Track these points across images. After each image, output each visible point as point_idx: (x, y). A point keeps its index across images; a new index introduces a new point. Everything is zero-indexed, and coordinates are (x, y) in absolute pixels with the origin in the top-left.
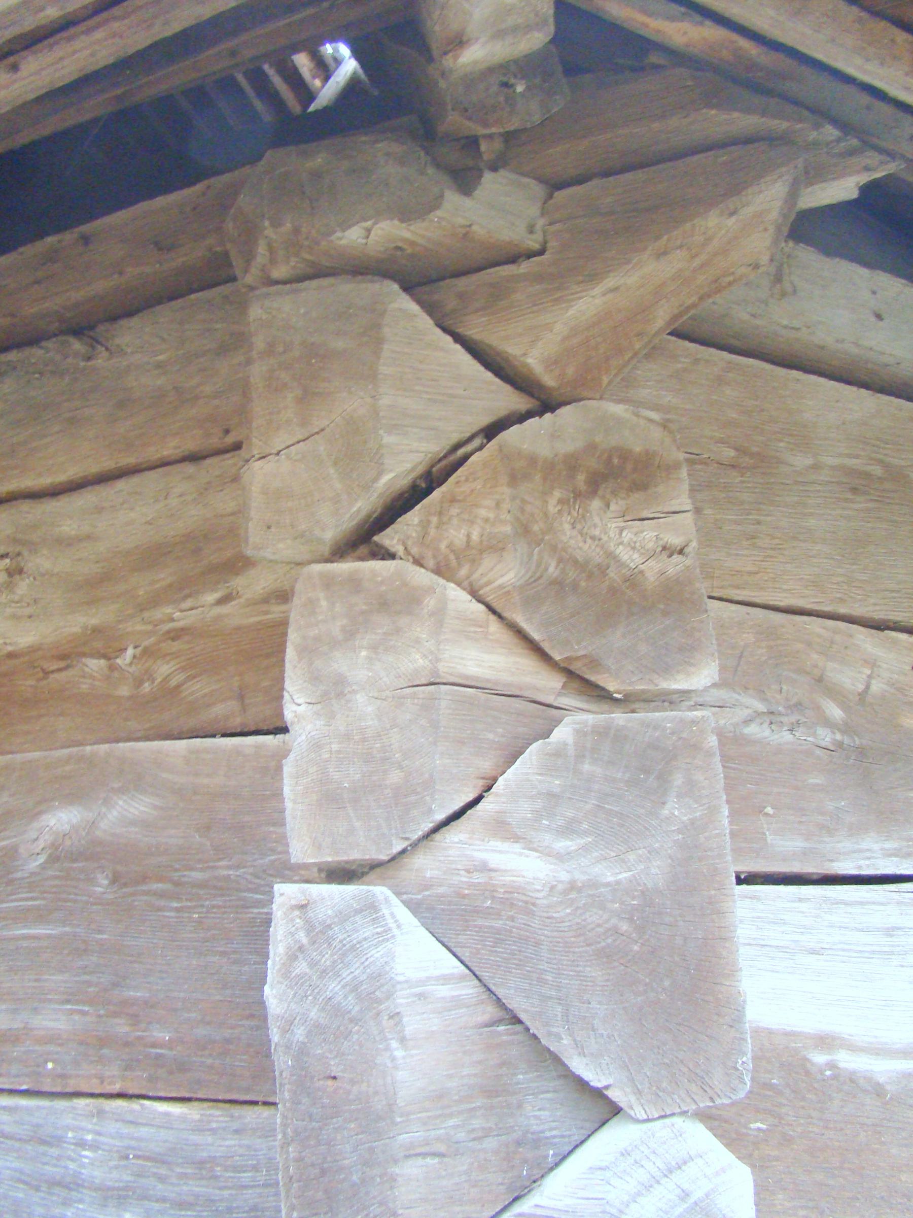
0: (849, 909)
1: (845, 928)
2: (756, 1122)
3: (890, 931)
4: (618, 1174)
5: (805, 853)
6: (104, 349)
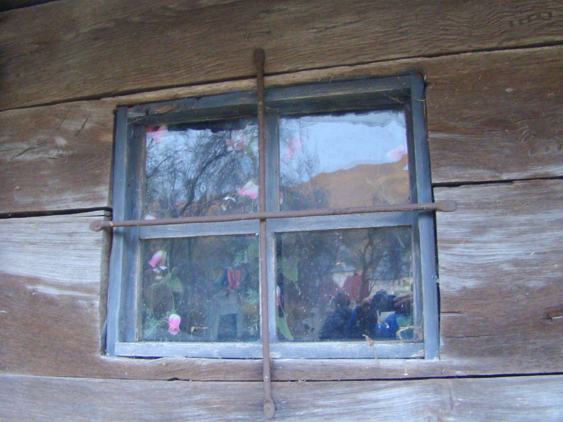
0: (52, 225)
1: (49, 233)
2: (3, 310)
3: (70, 234)
4: (272, 402)
5: (33, 203)
6: (429, 140)
